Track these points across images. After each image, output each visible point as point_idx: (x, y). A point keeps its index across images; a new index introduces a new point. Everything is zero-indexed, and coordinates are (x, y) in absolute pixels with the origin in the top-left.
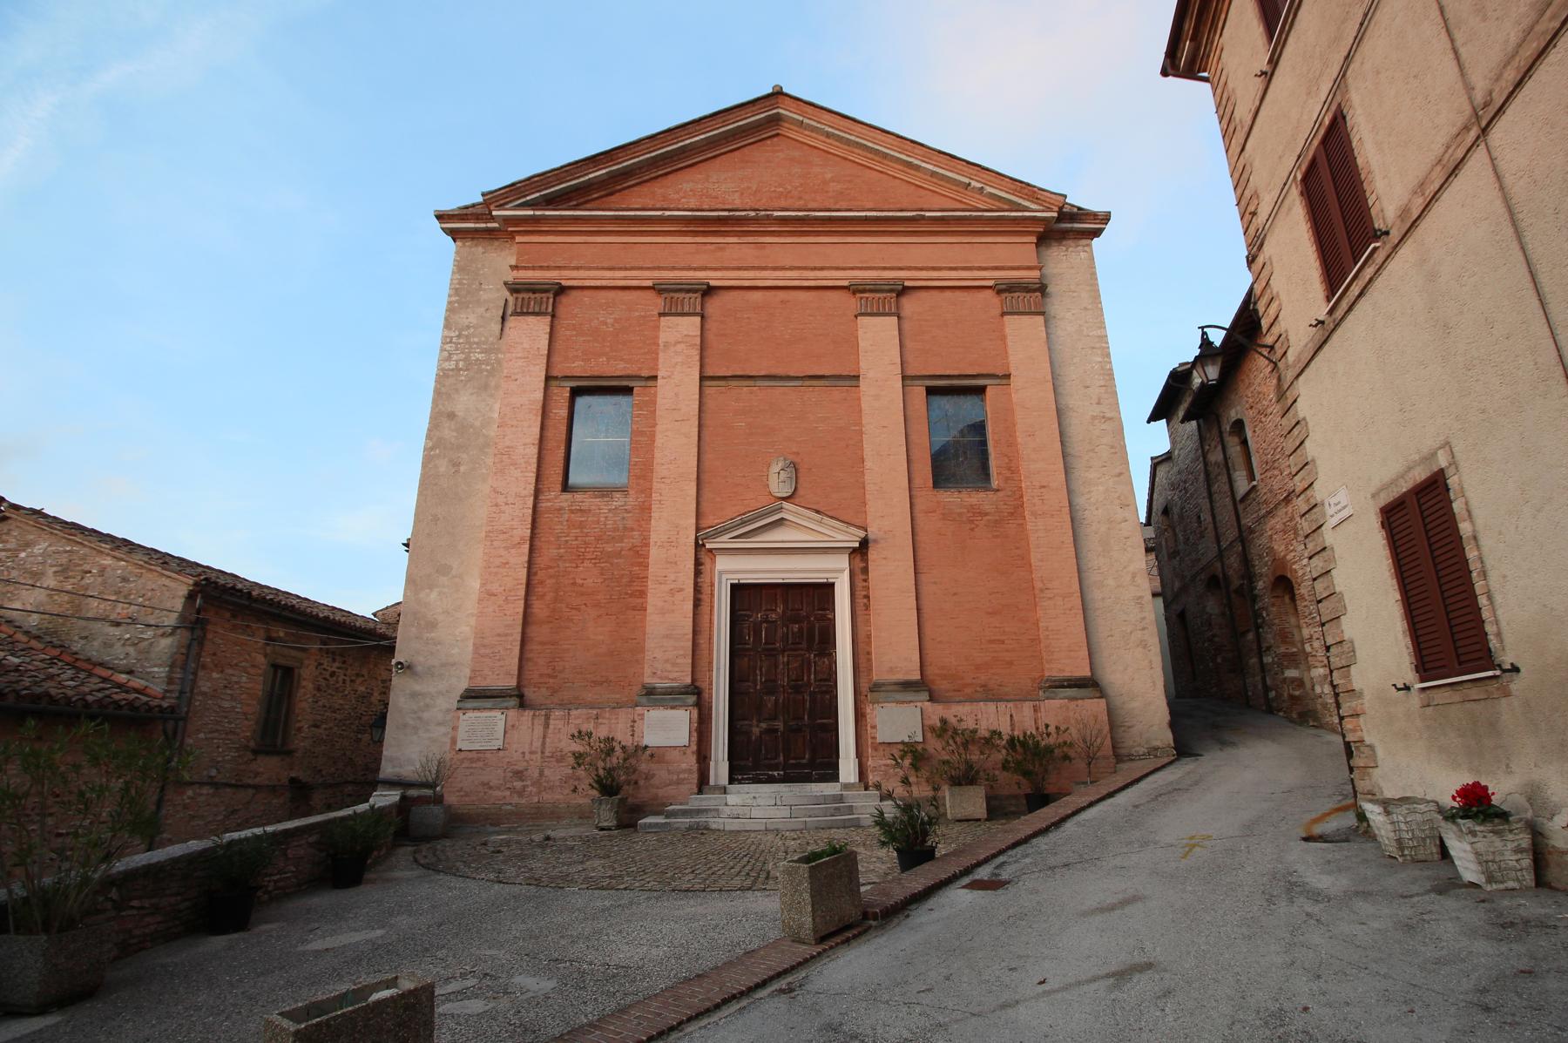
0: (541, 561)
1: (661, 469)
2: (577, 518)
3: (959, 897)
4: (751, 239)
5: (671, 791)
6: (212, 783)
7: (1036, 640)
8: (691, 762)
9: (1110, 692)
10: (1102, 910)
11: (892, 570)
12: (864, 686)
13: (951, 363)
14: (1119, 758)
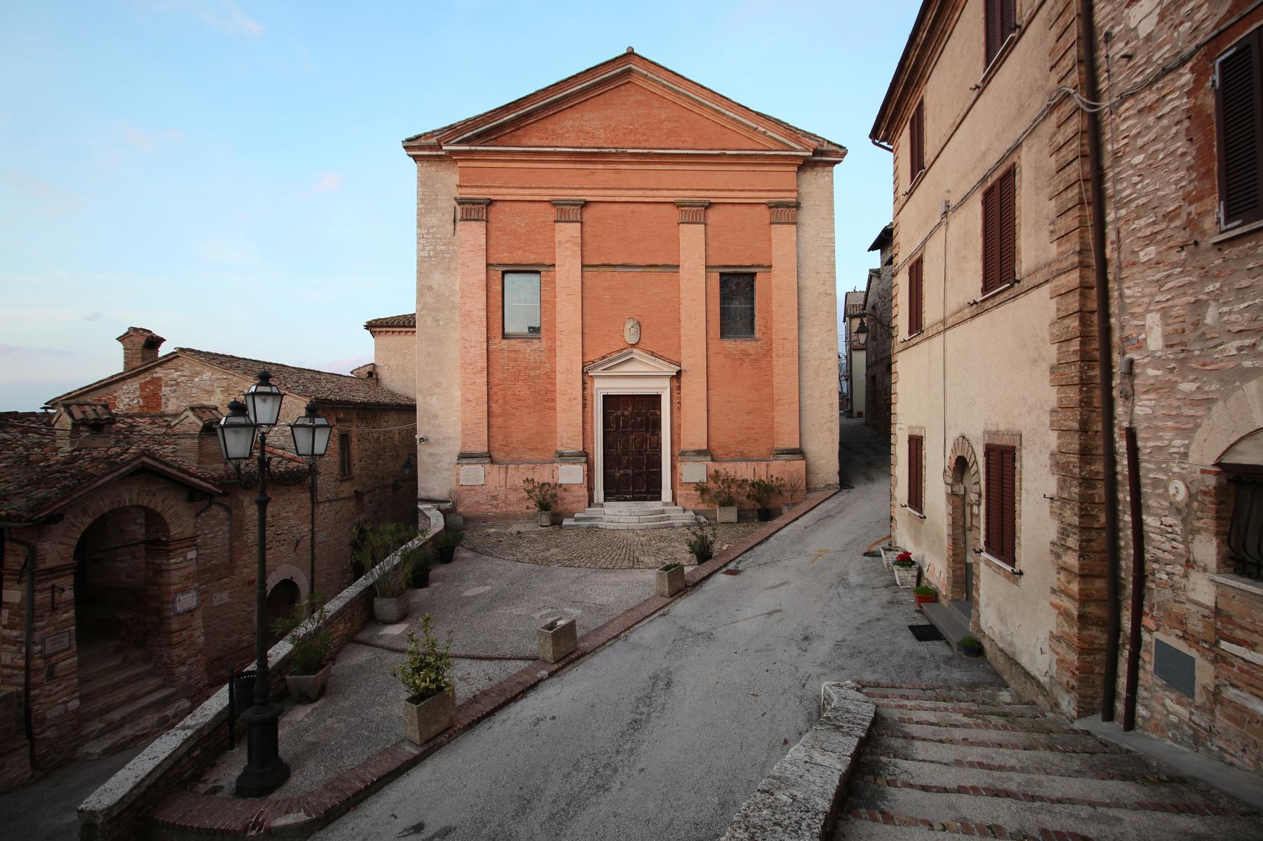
0: (495, 380)
1: (560, 327)
2: (513, 355)
3: (721, 578)
4: (611, 166)
5: (575, 506)
6: (329, 501)
7: (772, 428)
8: (585, 492)
9: (810, 455)
10: (772, 587)
11: (694, 387)
12: (676, 453)
13: (736, 258)
14: (809, 489)
